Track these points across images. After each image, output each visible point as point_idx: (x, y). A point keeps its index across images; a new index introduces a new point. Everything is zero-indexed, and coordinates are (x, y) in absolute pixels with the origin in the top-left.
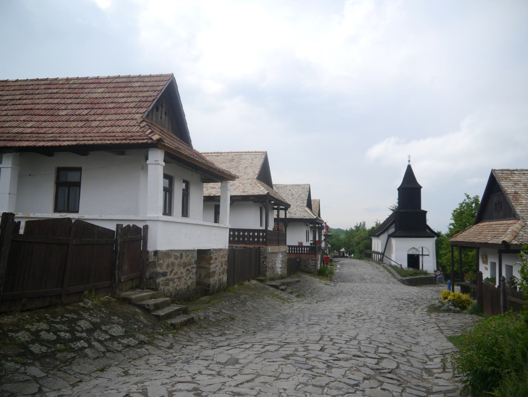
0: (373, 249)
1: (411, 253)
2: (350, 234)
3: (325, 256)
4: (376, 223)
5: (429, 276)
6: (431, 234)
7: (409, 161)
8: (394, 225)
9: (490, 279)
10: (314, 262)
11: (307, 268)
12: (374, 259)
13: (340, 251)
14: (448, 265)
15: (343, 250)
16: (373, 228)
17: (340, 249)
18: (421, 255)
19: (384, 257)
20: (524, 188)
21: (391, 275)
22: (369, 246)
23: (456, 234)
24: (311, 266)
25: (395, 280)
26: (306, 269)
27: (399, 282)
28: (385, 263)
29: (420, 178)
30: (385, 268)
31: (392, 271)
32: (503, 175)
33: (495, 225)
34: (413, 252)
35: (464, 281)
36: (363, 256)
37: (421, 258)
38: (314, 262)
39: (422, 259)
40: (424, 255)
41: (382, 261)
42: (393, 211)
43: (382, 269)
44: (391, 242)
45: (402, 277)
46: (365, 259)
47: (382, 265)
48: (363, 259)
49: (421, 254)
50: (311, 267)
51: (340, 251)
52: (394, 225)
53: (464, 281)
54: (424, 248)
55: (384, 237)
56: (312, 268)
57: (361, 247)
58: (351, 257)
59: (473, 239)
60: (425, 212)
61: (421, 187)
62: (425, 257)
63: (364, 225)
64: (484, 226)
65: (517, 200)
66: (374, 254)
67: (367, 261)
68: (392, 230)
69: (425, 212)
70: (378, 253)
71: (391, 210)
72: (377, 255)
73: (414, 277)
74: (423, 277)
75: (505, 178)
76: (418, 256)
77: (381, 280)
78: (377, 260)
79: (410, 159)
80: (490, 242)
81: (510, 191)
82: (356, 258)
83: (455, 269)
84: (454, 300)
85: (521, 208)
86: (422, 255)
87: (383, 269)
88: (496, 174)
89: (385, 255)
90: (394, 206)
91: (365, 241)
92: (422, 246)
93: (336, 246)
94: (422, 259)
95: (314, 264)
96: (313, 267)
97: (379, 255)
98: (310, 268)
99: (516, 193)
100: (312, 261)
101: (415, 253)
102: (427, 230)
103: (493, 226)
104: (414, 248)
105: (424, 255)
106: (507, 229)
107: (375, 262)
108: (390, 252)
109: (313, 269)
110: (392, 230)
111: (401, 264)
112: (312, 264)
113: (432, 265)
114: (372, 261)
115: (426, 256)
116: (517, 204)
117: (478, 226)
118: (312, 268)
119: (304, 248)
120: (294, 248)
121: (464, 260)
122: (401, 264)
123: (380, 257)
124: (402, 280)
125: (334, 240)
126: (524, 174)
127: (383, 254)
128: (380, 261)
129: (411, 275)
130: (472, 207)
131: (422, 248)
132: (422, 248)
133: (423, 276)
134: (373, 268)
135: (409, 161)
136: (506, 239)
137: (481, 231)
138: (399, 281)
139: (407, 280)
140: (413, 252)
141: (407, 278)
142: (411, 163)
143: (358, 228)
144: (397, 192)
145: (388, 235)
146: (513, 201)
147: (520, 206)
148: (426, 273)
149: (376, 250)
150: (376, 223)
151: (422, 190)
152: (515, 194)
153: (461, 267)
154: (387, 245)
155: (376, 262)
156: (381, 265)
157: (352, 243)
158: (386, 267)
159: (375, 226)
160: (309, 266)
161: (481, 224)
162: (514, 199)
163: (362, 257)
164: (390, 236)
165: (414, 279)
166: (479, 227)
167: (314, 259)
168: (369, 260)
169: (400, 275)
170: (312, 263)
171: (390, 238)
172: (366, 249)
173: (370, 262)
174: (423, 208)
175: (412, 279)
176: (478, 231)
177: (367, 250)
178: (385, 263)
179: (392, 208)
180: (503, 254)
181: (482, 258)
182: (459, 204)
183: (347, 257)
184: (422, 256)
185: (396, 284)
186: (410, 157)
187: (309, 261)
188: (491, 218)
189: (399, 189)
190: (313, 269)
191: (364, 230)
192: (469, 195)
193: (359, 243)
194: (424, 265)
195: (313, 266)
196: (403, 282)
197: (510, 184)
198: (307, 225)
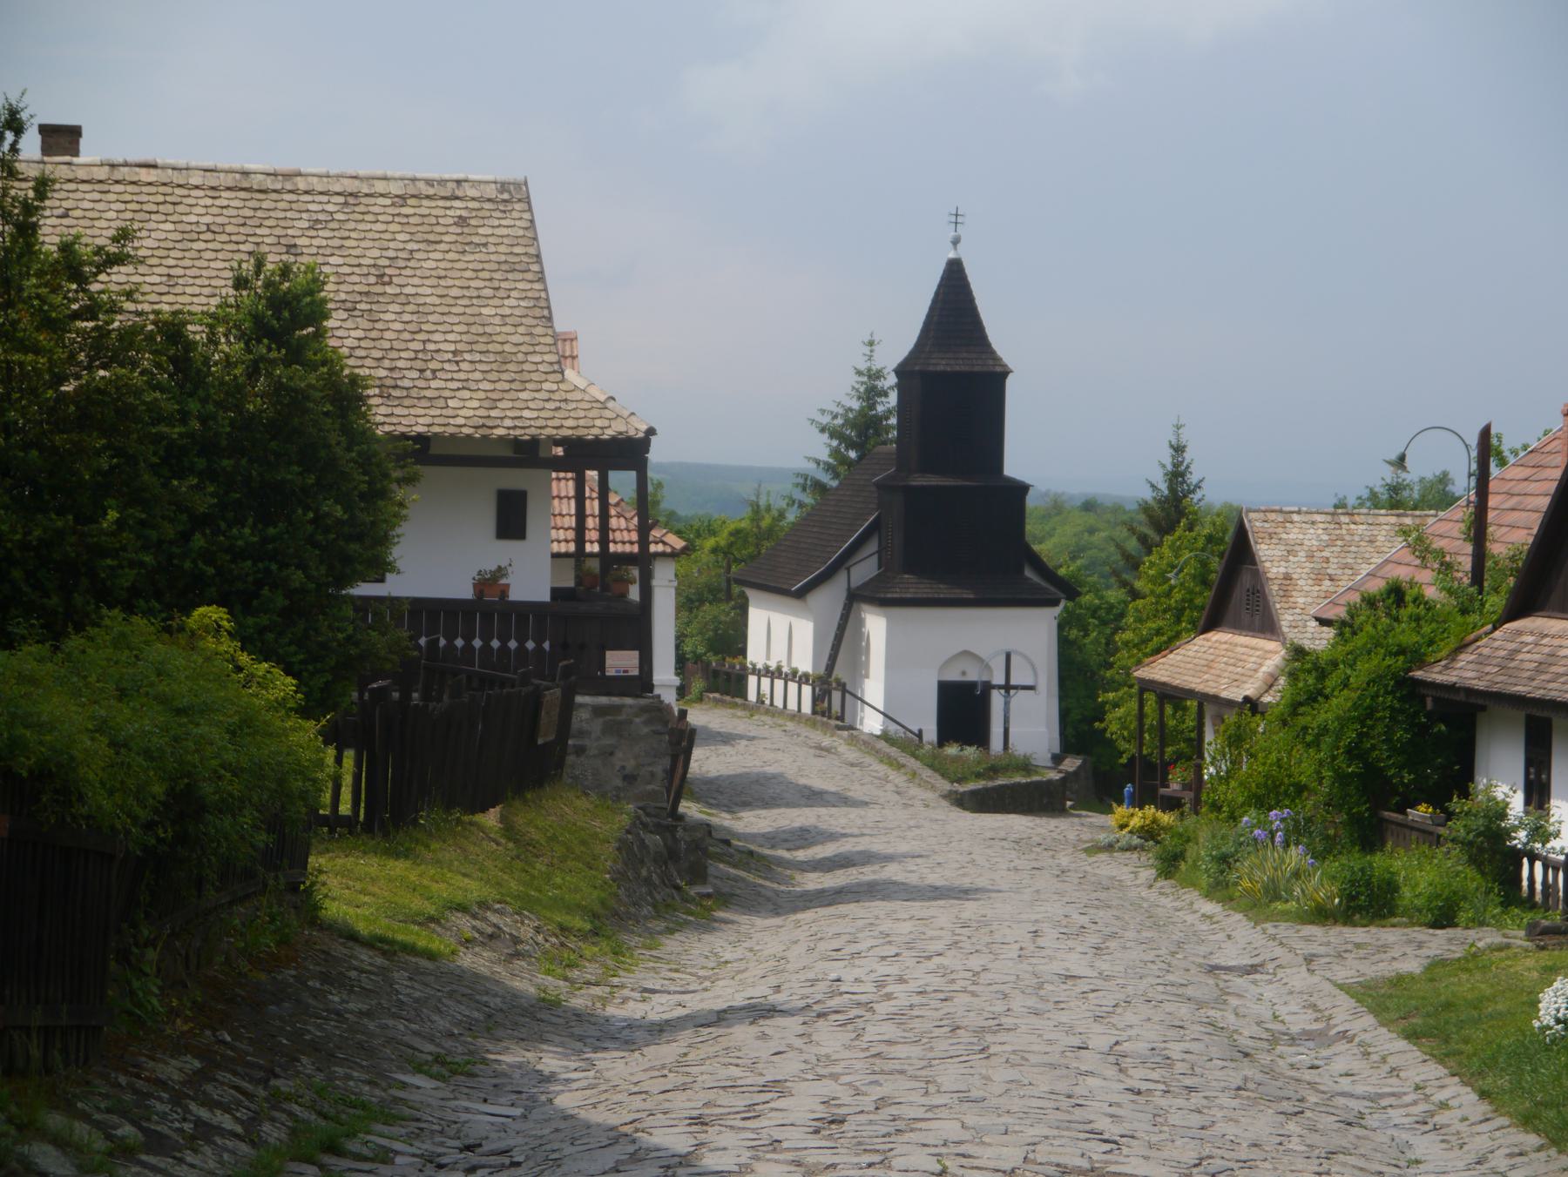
1: (953, 676)
5: (1036, 778)
8: (872, 546)
9: (603, 649)
14: (1124, 738)
18: (1000, 687)
20: (1307, 564)
21: (905, 778)
23: (1152, 655)
25: (929, 795)
27: (945, 803)
32: (1266, 525)
33: (1242, 646)
34: (964, 673)
35: (1168, 786)
37: (997, 699)
39: (1007, 704)
40: (1016, 688)
42: (832, 436)
44: (861, 623)
45: (952, 782)
46: (716, 701)
49: (999, 679)
52: (872, 546)
53: (1168, 786)
54: (1014, 659)
59: (1191, 679)
62: (1018, 698)
64: (1221, 643)
65: (1286, 595)
68: (865, 569)
71: (823, 430)
73: (990, 784)
74: (1019, 784)
75: (1270, 534)
76: (988, 687)
80: (1224, 694)
81: (1275, 570)
83: (1145, 752)
84: (1142, 827)
85: (1291, 618)
86: (1007, 687)
88: (1250, 521)
90: (841, 411)
92: (1008, 647)
94: (1007, 704)
97: (807, 690)
99: (1287, 577)
101: (973, 675)
102: (1029, 573)
103: (1239, 649)
104: (966, 654)
105: (1016, 688)
106: (1261, 665)
107: (767, 712)
108: (860, 668)
110: (865, 569)
113: (1043, 729)
115: (1022, 693)
116: (1287, 606)
117: (1208, 640)
121: (1172, 723)
124: (956, 792)
126: (1313, 523)
129: (979, 776)
133: (1019, 779)
136: (1248, 693)
137: (1212, 657)
138: (944, 797)
139: (973, 793)
140: (964, 673)
141: (971, 786)
145: (849, 589)
146: (1277, 599)
147: (1291, 611)
148: (1026, 766)
149: (777, 658)
151: (1011, 384)
152: (1285, 579)
153: (1163, 745)
156: (841, 737)
161: (1216, 636)
162: (1281, 593)
164: (857, 597)
165: (994, 789)
166: (1210, 644)
175: (986, 790)
176: (1205, 656)
179: (826, 420)
180: (636, 672)
181: (1214, 725)
184: (1007, 691)
185: (934, 808)
188: (1239, 627)
194: (1011, 730)
197: (1278, 551)
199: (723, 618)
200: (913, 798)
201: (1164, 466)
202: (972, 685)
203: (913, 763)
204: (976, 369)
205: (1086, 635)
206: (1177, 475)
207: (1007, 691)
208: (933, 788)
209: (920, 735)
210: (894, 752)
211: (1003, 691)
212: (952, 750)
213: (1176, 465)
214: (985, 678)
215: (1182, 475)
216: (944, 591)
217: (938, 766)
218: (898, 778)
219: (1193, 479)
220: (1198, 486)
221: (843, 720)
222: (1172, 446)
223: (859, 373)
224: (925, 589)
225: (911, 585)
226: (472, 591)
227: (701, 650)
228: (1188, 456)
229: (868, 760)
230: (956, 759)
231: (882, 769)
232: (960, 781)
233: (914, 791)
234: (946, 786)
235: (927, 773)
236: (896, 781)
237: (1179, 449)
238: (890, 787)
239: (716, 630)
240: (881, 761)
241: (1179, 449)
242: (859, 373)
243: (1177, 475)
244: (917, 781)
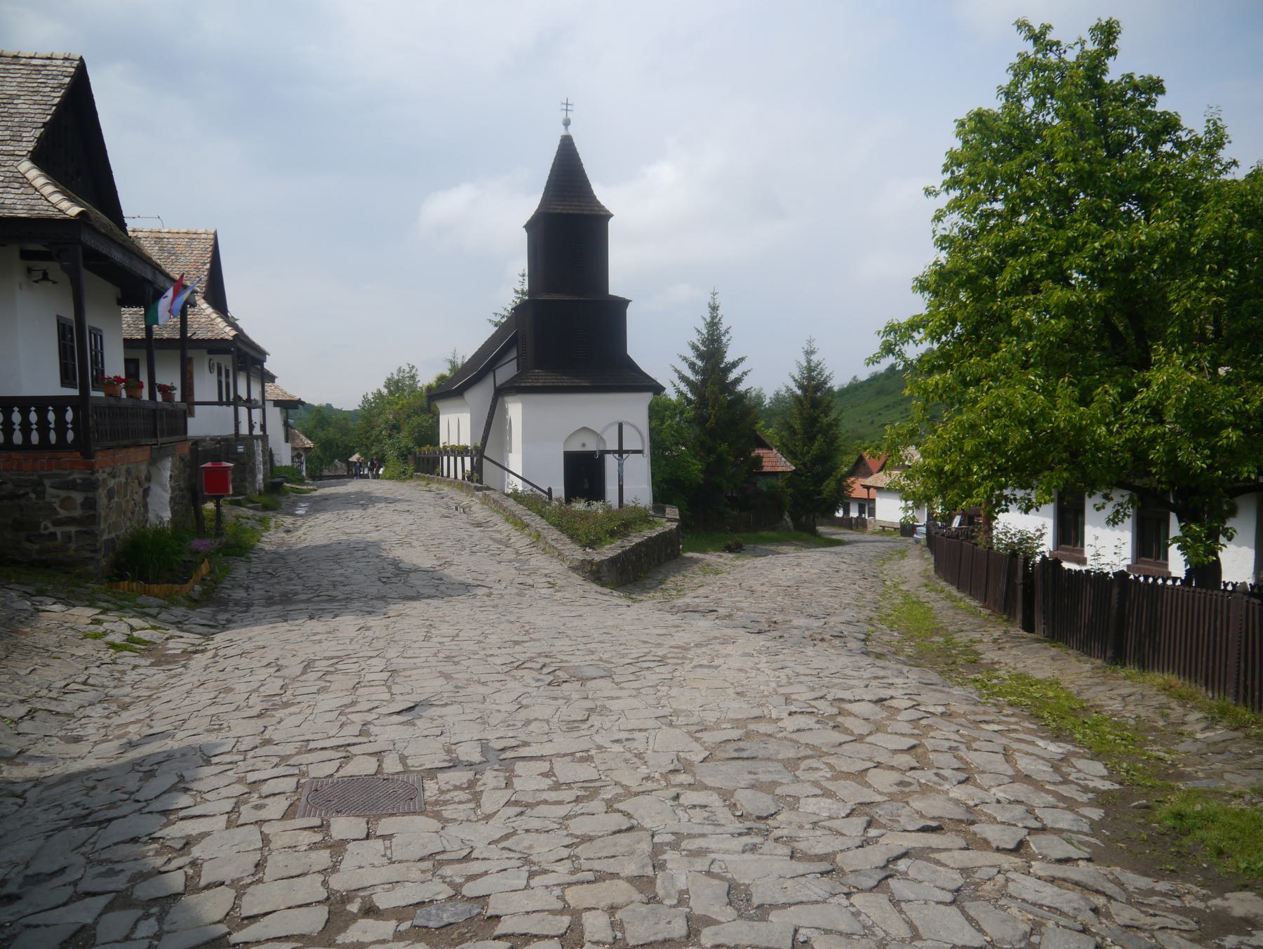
0: (443, 439)
1: (576, 447)
2: (372, 410)
3: (209, 465)
4: (451, 362)
6: (632, 379)
7: (567, 123)
8: (514, 354)
10: (78, 497)
11: (29, 540)
12: (445, 474)
13: (351, 460)
15: (355, 458)
16: (442, 378)
17: (351, 456)
18: (614, 452)
19: (484, 460)
21: (528, 541)
22: (430, 435)
24: (58, 523)
26: (27, 545)
27: (576, 579)
28: (488, 488)
29: (604, 193)
30: (498, 507)
31: (527, 519)
34: (584, 445)
36: (411, 469)
37: (611, 463)
38: (78, 497)
39: (620, 465)
40: (627, 452)
41: (480, 481)
43: (479, 511)
44: (505, 411)
45: (584, 546)
46: (418, 477)
47: (480, 494)
48: (411, 477)
50: (59, 531)
51: (351, 460)
52: (514, 354)
55: (481, 395)
56: (68, 537)
57: (404, 439)
58: (377, 476)
60: (622, 304)
61: (609, 216)
62: (630, 460)
63: (413, 377)
66: (445, 458)
67: (424, 483)
68: (507, 371)
69: (622, 304)
70: (461, 451)
72: (459, 459)
77: (487, 574)
78: (460, 476)
79: (570, 115)
82: (390, 478)
86: (621, 452)
87: (487, 513)
89: (485, 454)
91: (416, 420)
92: (620, 420)
93: (338, 447)
94: (620, 465)
95: (78, 513)
96: (73, 529)
97: (468, 460)
98: (53, 535)
100: (63, 494)
101: (591, 446)
104: (585, 429)
107: (450, 484)
108: (505, 446)
109: (73, 546)
110: (507, 371)
111: (550, 489)
112: (63, 513)
113: (646, 486)
114: (439, 482)
118: (68, 537)
119: (25, 414)
120: (25, 414)
122: (550, 489)
123: (468, 467)
124: (591, 562)
125: (331, 432)
127: (478, 453)
128: (470, 479)
130: (999, 150)
131: (620, 426)
132: (620, 426)
134: (444, 511)
135: (567, 123)
138: (574, 569)
140: (584, 445)
142: (572, 131)
143: (395, 386)
144: (524, 235)
149: (454, 442)
150: (451, 362)
154: (492, 423)
155: (454, 483)
156: (477, 497)
157: (375, 433)
158: (495, 501)
159: (447, 373)
160: (47, 526)
163: (409, 472)
164: (502, 392)
167: (77, 476)
168: (429, 481)
169: (573, 537)
170: (66, 503)
171: (500, 399)
172: (420, 446)
173: (434, 486)
174: (616, 287)
177: (424, 449)
178: (488, 488)
182: (1019, 54)
183: (366, 477)
184: (621, 455)
186: (569, 108)
187: (41, 495)
189: (530, 226)
190: (73, 546)
191: (413, 389)
192: (1046, 28)
193: (396, 427)
195: (71, 521)
196: (596, 574)
198: (45, 277)
199: (424, 424)
200: (534, 572)
201: (705, 319)
202: (592, 453)
203: (537, 522)
204: (585, 212)
205: (663, 423)
206: (713, 325)
207: (621, 455)
208: (560, 556)
209: (549, 492)
210: (519, 509)
211: (617, 455)
212: (580, 506)
213: (713, 318)
214: (602, 448)
215: (716, 324)
216: (567, 381)
217: (566, 525)
218: (520, 541)
219: (723, 328)
220: (727, 332)
221: (481, 483)
222: (710, 306)
223: (516, 292)
224: (551, 380)
225: (543, 379)
226: (112, 376)
227: (411, 445)
228: (720, 313)
229: (496, 518)
230: (584, 516)
231: (505, 528)
232: (593, 544)
233: (539, 560)
234: (577, 553)
235: (553, 535)
236: (518, 545)
237: (714, 308)
238: (509, 554)
239: (420, 432)
240: (507, 520)
241: (714, 308)
242: (516, 292)
243: (713, 325)
244: (541, 545)
